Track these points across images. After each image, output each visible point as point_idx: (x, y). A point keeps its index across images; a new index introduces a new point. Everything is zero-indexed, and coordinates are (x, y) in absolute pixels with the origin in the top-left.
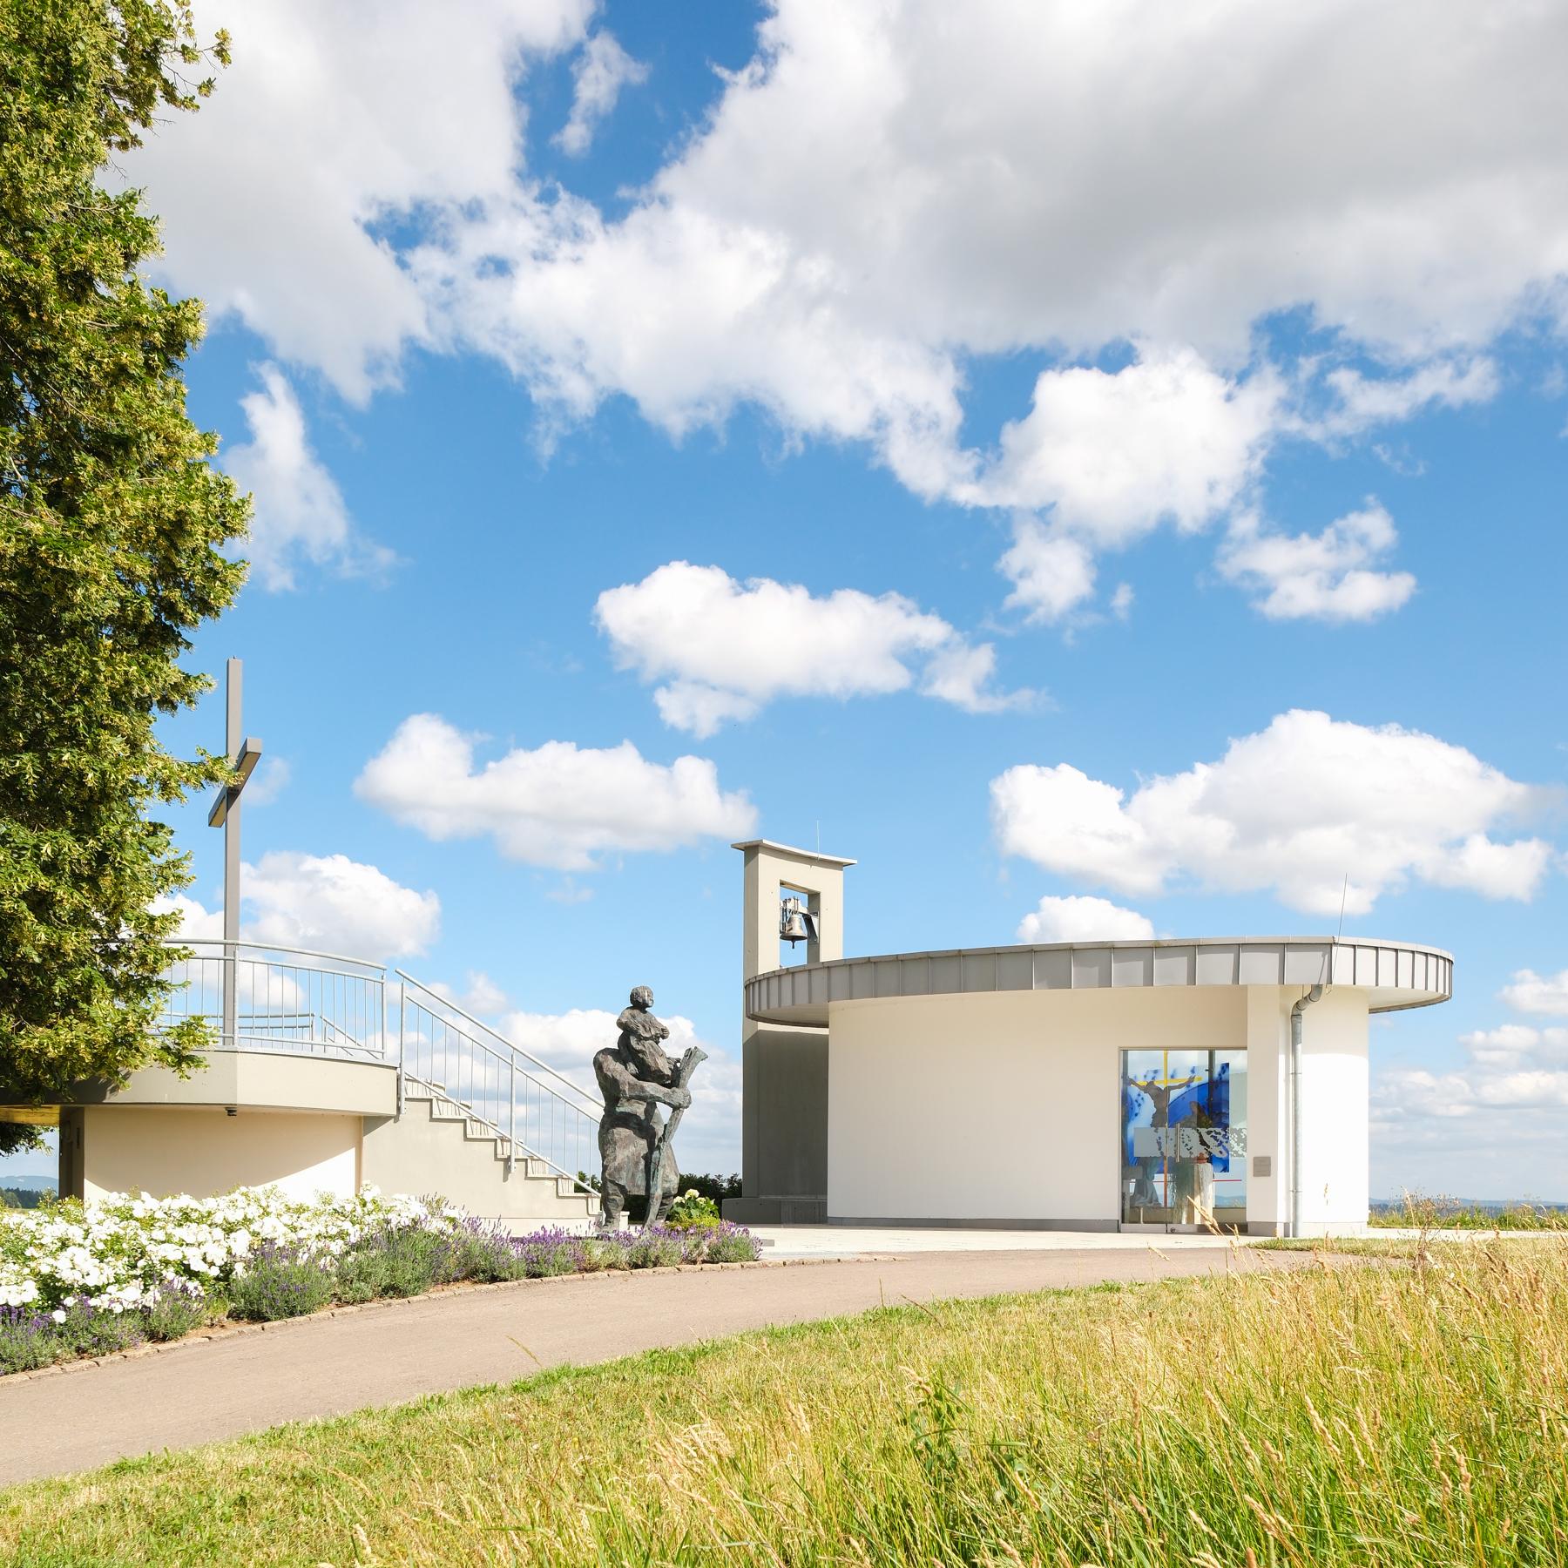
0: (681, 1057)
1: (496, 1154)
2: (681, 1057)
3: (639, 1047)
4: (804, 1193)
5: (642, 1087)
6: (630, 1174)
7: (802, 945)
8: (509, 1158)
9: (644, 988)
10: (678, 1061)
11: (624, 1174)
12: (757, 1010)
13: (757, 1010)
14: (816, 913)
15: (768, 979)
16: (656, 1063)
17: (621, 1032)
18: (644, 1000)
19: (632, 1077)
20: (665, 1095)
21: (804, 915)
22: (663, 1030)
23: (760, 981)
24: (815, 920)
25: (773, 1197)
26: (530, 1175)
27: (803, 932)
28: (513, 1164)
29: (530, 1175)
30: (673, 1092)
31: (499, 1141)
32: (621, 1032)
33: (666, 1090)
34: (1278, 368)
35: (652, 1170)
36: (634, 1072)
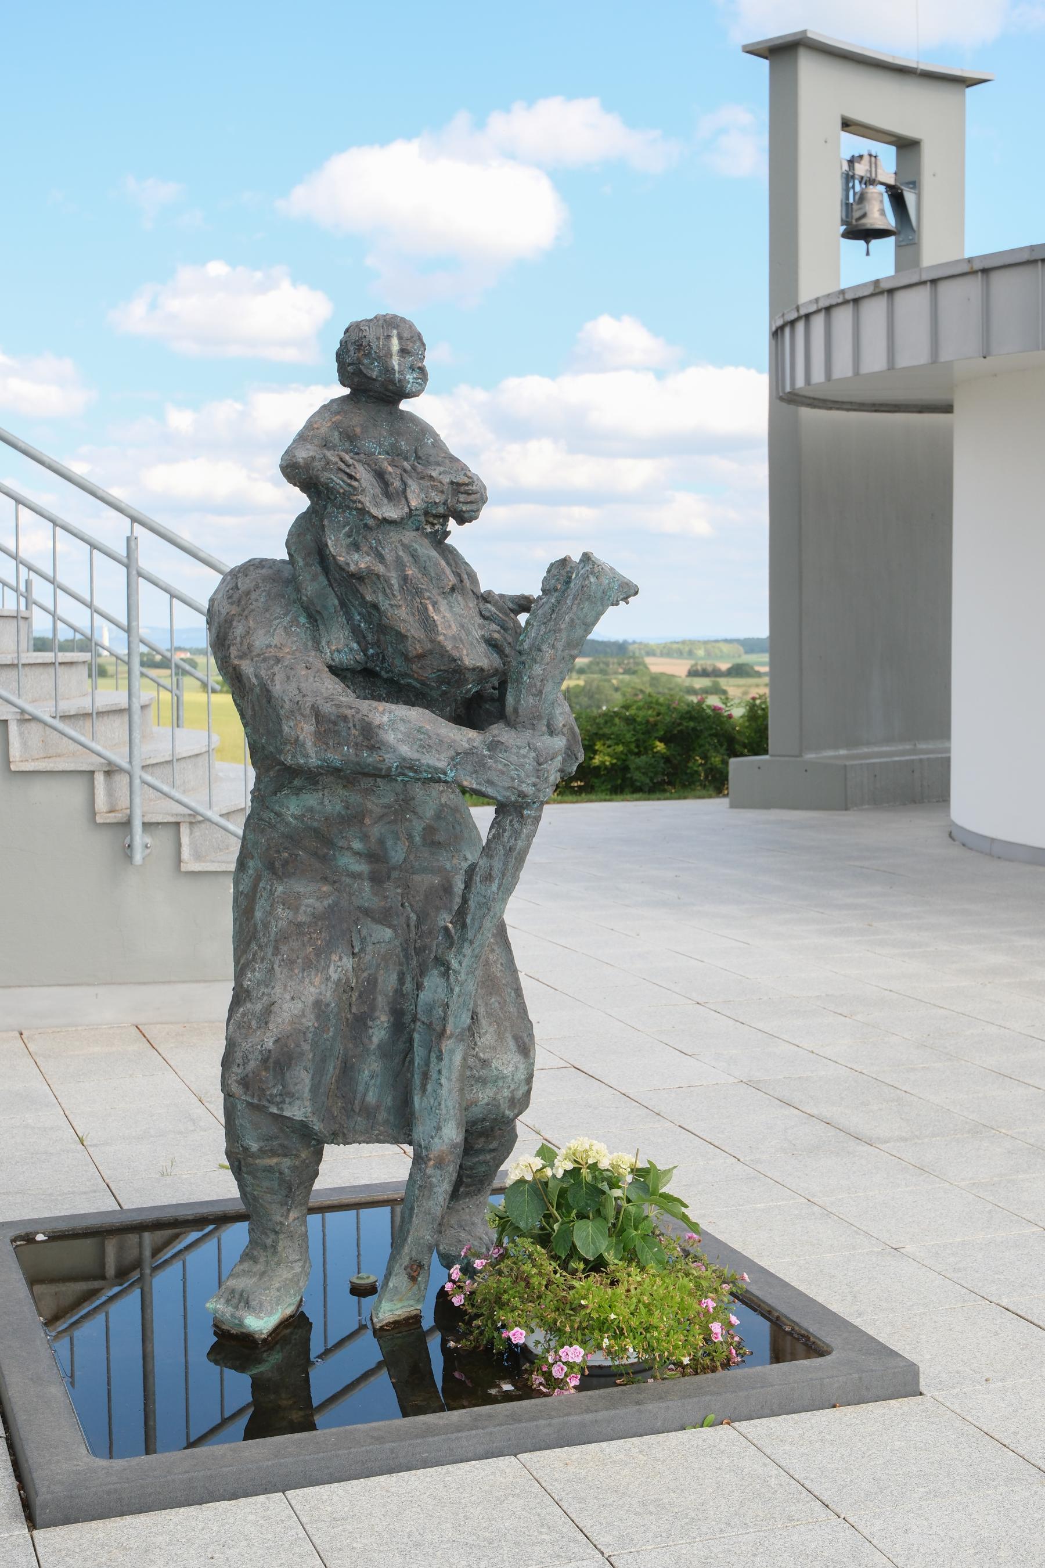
0: (536, 592)
1: (93, 813)
2: (536, 592)
3: (360, 562)
4: (888, 740)
5: (368, 733)
6: (332, 1069)
7: (885, 247)
8: (126, 825)
9: (390, 323)
10: (524, 604)
11: (302, 1078)
12: (800, 383)
13: (800, 383)
14: (915, 185)
15: (828, 309)
16: (428, 624)
17: (300, 501)
18: (388, 370)
19: (331, 686)
20: (460, 758)
21: (889, 187)
22: (457, 488)
23: (807, 316)
24: (910, 198)
25: (830, 753)
26: (190, 864)
27: (890, 221)
28: (139, 837)
29: (190, 864)
30: (494, 746)
31: (100, 779)
32: (300, 501)
33: (465, 737)
34: (500, 670)
35: (419, 1053)
36: (344, 658)
